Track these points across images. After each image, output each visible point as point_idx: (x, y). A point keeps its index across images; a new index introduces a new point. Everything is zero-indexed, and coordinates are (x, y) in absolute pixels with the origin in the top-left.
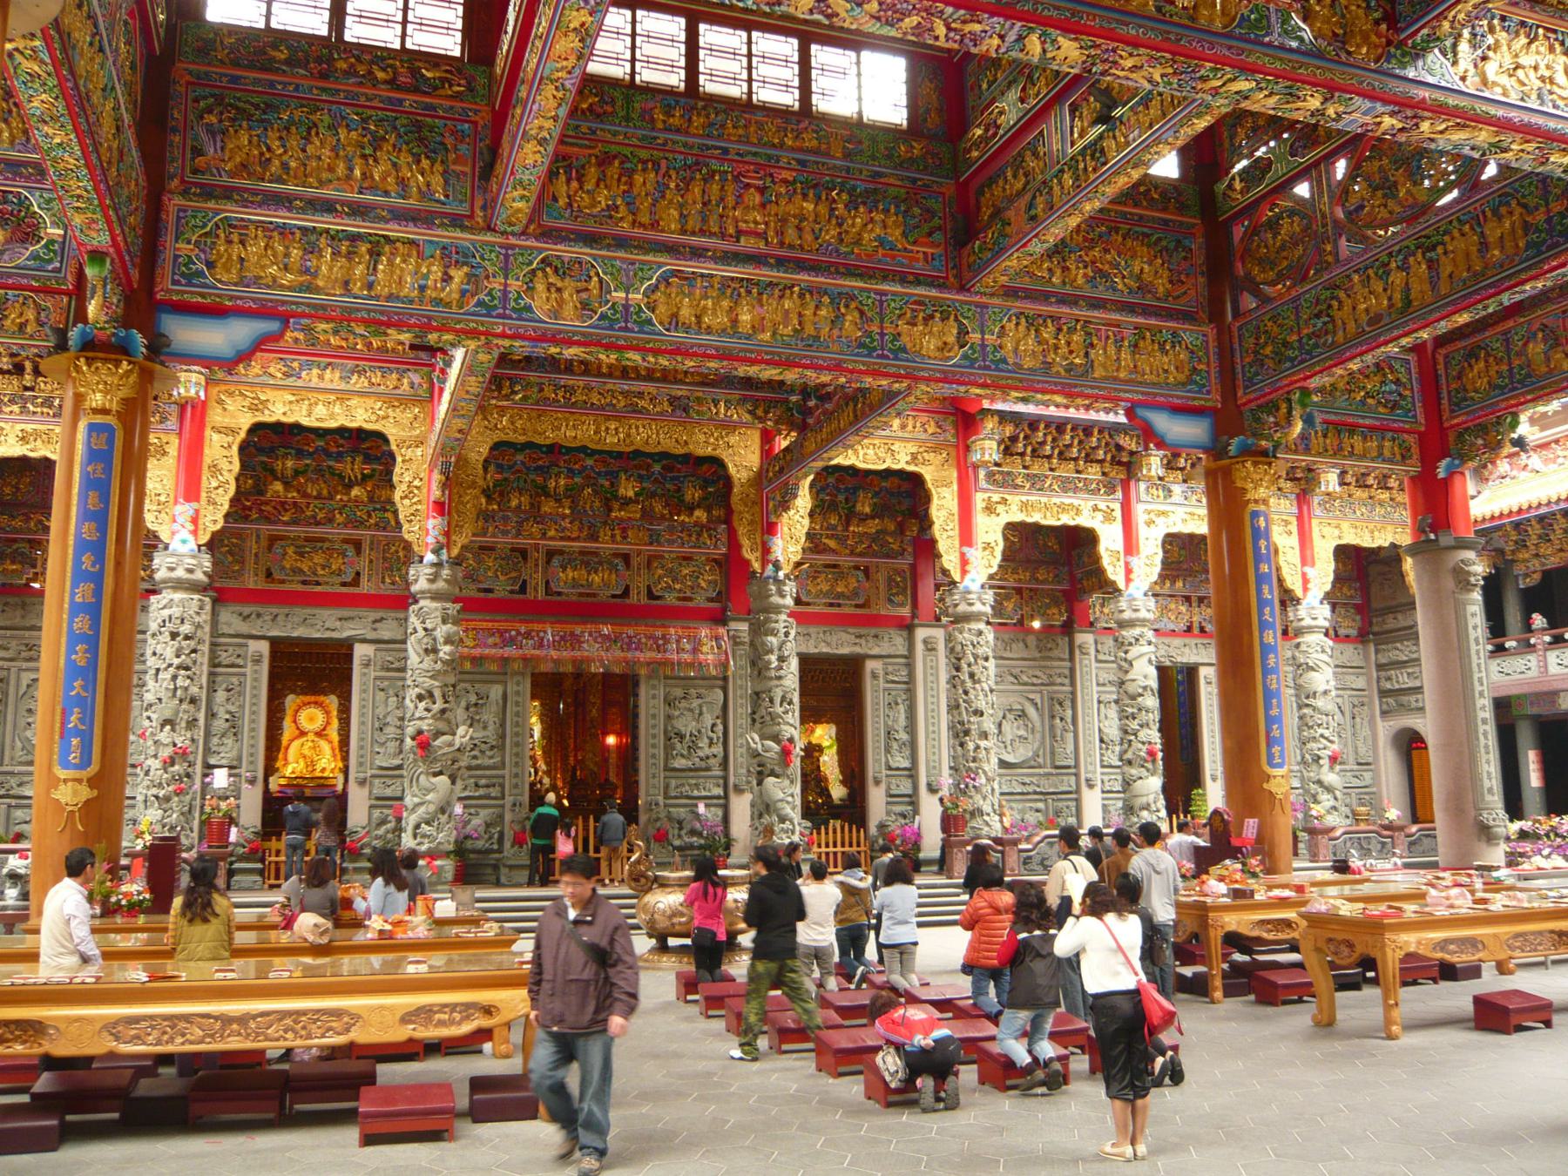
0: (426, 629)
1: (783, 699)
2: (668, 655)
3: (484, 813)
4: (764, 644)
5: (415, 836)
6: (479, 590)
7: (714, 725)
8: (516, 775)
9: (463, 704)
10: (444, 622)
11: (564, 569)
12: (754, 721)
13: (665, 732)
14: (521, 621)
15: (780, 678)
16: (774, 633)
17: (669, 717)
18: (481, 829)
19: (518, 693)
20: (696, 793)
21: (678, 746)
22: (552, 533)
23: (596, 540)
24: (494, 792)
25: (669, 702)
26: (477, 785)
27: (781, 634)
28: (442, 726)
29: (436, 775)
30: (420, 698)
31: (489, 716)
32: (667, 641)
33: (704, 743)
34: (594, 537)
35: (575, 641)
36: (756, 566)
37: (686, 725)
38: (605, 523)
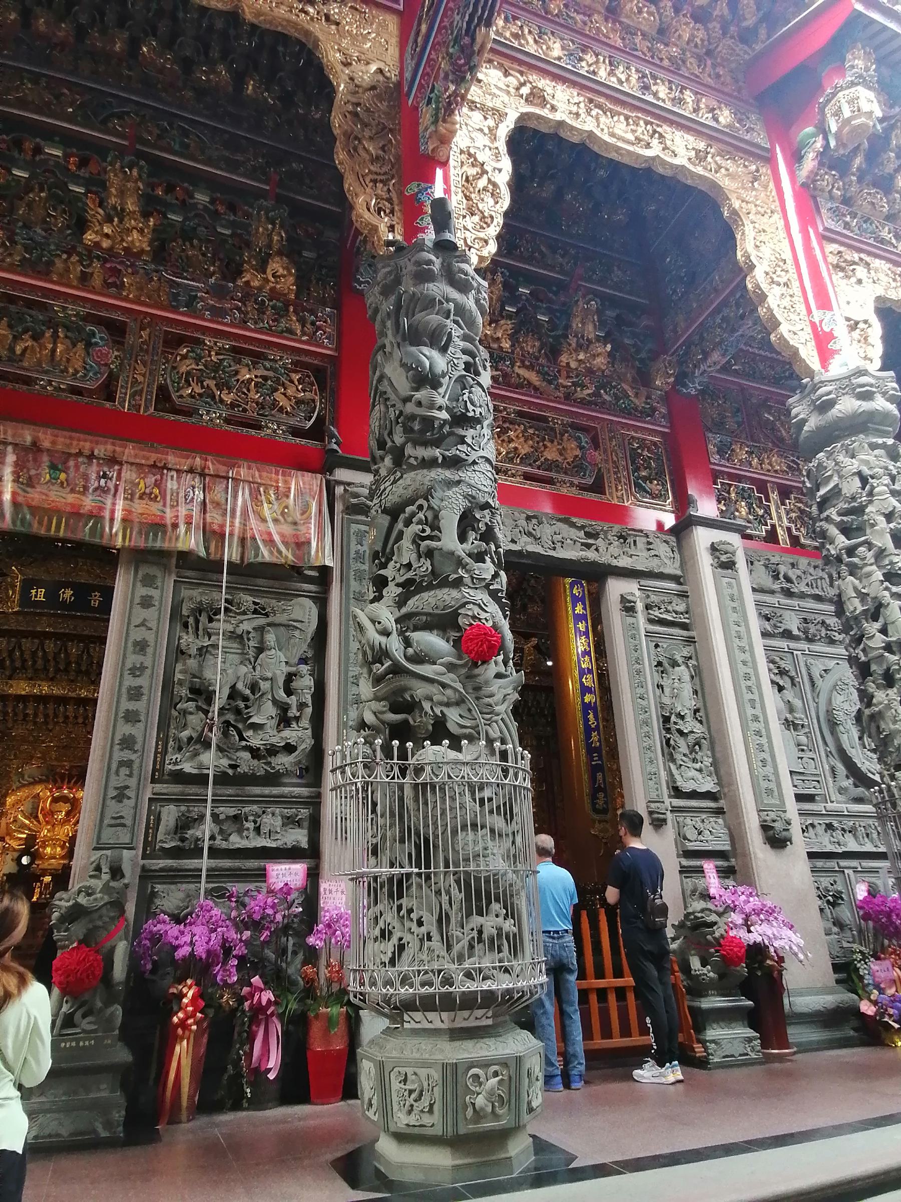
1: (466, 522)
7: (290, 678)
13: (168, 684)
23: (45, 274)
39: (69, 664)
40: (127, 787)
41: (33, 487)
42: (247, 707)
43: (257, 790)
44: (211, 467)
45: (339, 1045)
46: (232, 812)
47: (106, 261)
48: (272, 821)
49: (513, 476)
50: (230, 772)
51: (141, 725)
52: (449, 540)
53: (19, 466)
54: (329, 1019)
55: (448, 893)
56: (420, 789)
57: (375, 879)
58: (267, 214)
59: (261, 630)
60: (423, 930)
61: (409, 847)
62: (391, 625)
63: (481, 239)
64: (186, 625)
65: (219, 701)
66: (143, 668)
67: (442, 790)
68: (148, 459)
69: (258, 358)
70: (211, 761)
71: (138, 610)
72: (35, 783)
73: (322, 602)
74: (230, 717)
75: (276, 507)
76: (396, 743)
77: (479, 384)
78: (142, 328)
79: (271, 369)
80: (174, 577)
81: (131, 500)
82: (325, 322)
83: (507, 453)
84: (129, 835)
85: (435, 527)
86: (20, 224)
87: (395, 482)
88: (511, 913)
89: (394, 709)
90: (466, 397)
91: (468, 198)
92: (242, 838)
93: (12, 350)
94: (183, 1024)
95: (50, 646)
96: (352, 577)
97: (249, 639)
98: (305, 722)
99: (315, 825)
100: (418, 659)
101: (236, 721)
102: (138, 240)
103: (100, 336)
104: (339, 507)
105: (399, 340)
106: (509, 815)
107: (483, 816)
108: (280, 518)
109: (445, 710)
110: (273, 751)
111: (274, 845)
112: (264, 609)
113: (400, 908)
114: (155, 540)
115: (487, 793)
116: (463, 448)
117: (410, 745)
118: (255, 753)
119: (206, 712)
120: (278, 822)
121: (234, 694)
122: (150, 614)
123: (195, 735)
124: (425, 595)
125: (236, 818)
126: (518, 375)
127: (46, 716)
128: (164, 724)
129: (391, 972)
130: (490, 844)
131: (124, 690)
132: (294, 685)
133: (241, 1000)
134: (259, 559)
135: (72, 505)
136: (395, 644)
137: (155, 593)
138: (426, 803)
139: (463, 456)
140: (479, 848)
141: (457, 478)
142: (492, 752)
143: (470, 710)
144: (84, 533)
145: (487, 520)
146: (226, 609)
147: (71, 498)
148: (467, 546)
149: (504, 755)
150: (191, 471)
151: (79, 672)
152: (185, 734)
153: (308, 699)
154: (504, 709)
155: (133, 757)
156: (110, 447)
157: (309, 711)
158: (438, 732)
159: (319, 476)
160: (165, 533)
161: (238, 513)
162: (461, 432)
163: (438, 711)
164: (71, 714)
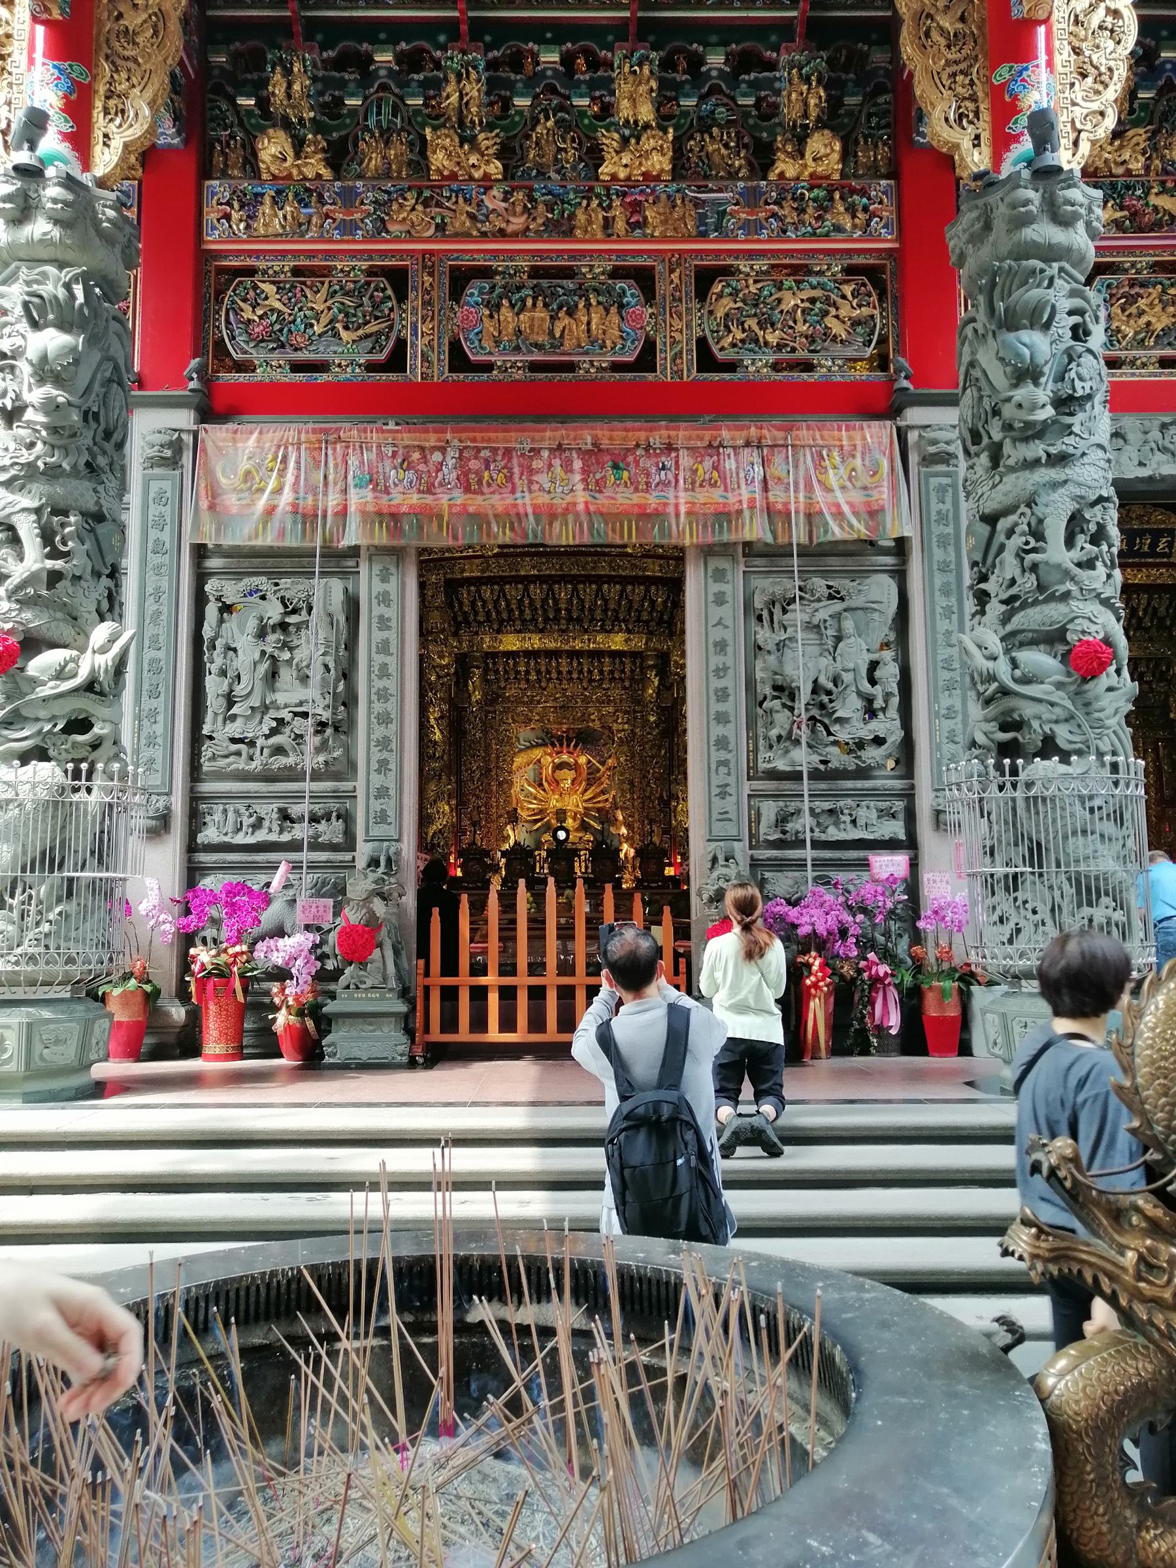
1: (1075, 524)
6: (296, 367)
7: (873, 666)
9: (252, 625)
11: (494, 308)
12: (982, 598)
13: (751, 684)
19: (384, 599)
22: (461, 222)
23: (569, 233)
24: (331, 831)
31: (313, 646)
33: (849, 707)
34: (562, 227)
36: (977, 159)
38: (588, 194)
39: (558, 611)
41: (600, 492)
42: (831, 701)
43: (849, 784)
44: (770, 435)
45: (953, 1012)
46: (827, 805)
47: (625, 194)
48: (867, 813)
49: (1144, 365)
50: (822, 767)
51: (731, 726)
52: (1056, 552)
53: (586, 471)
54: (942, 992)
55: (1060, 888)
56: (1032, 802)
57: (992, 875)
58: (800, 69)
59: (837, 617)
60: (1038, 917)
61: (1023, 849)
62: (996, 646)
63: (1095, 112)
64: (760, 618)
65: (805, 695)
67: (1053, 800)
68: (702, 439)
69: (800, 271)
70: (803, 758)
71: (713, 608)
72: (532, 747)
73: (900, 575)
74: (815, 712)
75: (842, 471)
76: (1007, 761)
77: (1089, 351)
78: (672, 271)
79: (820, 286)
80: (742, 568)
81: (693, 490)
82: (881, 203)
83: (1136, 333)
85: (1039, 536)
86: (534, 172)
87: (994, 486)
88: (1120, 905)
89: (1004, 728)
90: (1073, 374)
91: (1077, 51)
93: (551, 333)
94: (815, 985)
95: (536, 591)
96: (935, 545)
98: (893, 712)
99: (910, 817)
100: (1026, 680)
102: (660, 162)
103: (630, 291)
104: (913, 458)
105: (993, 327)
106: (1119, 818)
107: (1092, 822)
108: (848, 484)
109: (1054, 726)
110: (860, 744)
113: (1016, 899)
114: (721, 532)
115: (1097, 803)
116: (1070, 440)
117: (1020, 761)
119: (792, 709)
121: (816, 689)
122: (725, 611)
123: (784, 733)
124: (1030, 611)
125: (831, 812)
126: (1156, 208)
127: (539, 672)
128: (751, 724)
129: (1009, 949)
130: (1099, 846)
131: (712, 693)
132: (878, 674)
133: (859, 971)
134: (830, 538)
135: (639, 506)
136: (1002, 668)
137: (726, 588)
138: (1037, 813)
139: (1071, 450)
140: (1089, 851)
141: (1064, 477)
142: (1103, 765)
143: (1079, 726)
144: (655, 536)
146: (801, 598)
147: (636, 498)
148: (1075, 554)
149: (1115, 767)
150: (748, 444)
151: (570, 619)
152: (774, 733)
153: (894, 688)
154: (1115, 722)
155: (729, 756)
156: (664, 433)
157: (895, 701)
158: (1049, 748)
159: (888, 423)
160: (729, 522)
161: (802, 486)
162: (1068, 420)
163: (1047, 729)
164: (564, 669)
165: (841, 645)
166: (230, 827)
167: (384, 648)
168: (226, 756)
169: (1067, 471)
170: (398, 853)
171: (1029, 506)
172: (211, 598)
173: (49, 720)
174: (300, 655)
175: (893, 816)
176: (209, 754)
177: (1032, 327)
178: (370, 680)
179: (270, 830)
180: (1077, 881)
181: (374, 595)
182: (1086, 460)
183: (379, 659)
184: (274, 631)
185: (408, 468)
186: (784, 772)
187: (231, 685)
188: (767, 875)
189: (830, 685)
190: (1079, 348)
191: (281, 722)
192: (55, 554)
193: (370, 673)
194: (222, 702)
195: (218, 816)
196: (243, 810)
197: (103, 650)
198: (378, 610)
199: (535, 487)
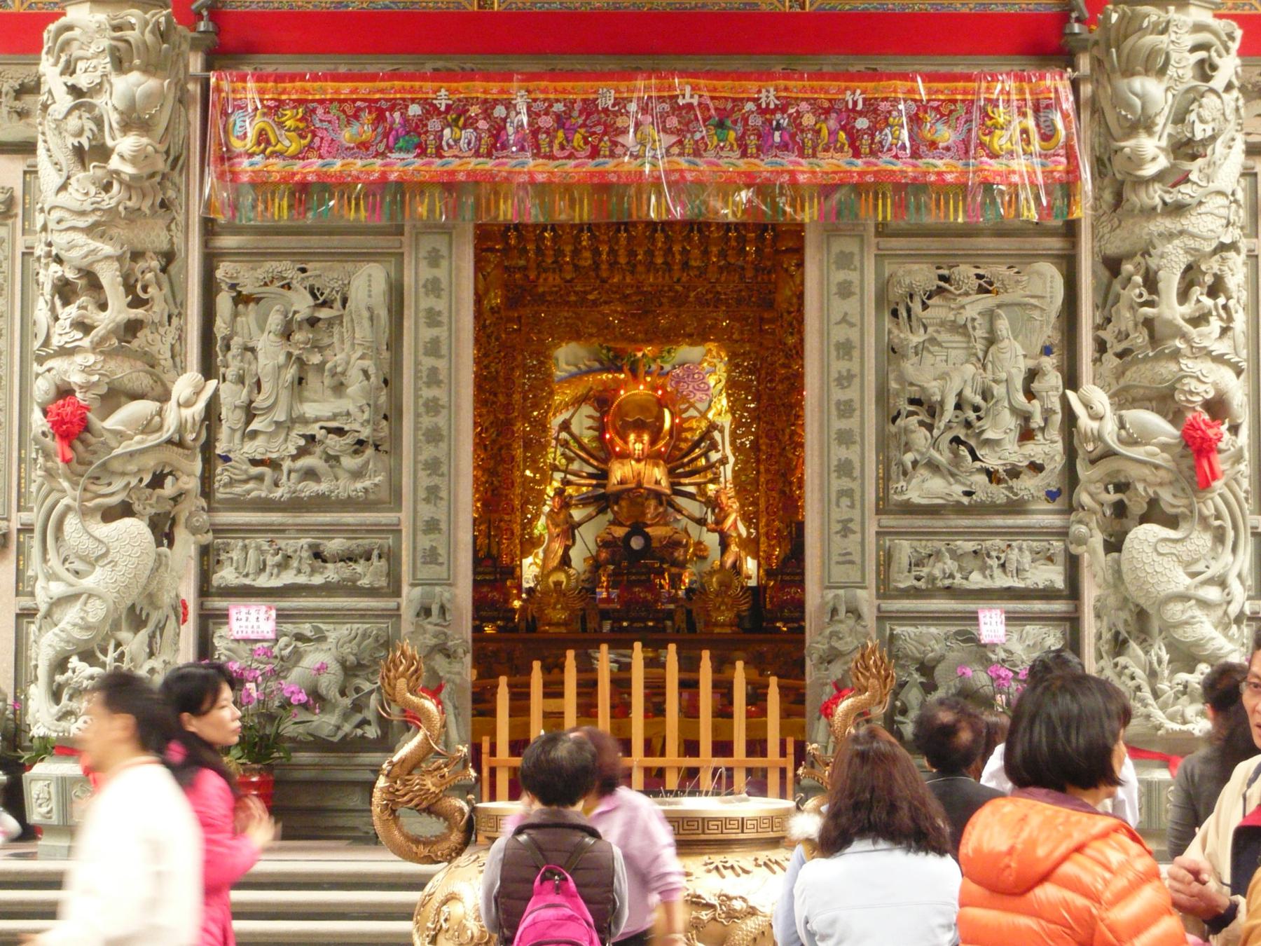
0: (74, 90)
1: (1190, 276)
2: (884, 162)
3: (337, 633)
4: (1119, 101)
5: (56, 696)
8: (432, 526)
9: (275, 320)
10: (120, 63)
13: (883, 395)
14: (437, 75)
15: (1179, 209)
16: (1157, 65)
17: (893, 352)
18: (329, 684)
19: (434, 287)
20: (977, 580)
21: (921, 437)
24: (367, 573)
25: (894, 307)
26: (317, 555)
27: (1184, 64)
28: (125, 371)
29: (109, 515)
30: (65, 291)
31: (351, 353)
32: (880, 120)
33: (1001, 427)
35: (601, 128)
37: (946, 373)
40: (851, 520)
41: (700, 156)
42: (979, 418)
43: (998, 521)
46: (970, 546)
48: (1020, 554)
50: (965, 500)
64: (895, 313)
66: (850, 376)
77: (1212, 90)
84: (859, 573)
92: (985, 577)
97: (974, 328)
98: (1055, 433)
100: (1133, 442)
101: (967, 435)
110: (1014, 473)
111: (1022, 585)
112: (991, 284)
116: (1185, 188)
118: (991, 475)
119: (930, 428)
120: (1027, 558)
128: (883, 443)
132: (1035, 386)
137: (853, 276)
139: (1188, 200)
141: (1179, 227)
145: (1216, 269)
148: (1188, 309)
152: (909, 458)
162: (1187, 165)
163: (1151, 492)
165: (993, 349)
166: (251, 567)
167: (433, 349)
168: (246, 481)
169: (1184, 221)
170: (453, 599)
171: (1143, 255)
172: (224, 286)
173: (135, 474)
174: (337, 359)
175: (1050, 559)
176: (225, 479)
177: (1147, 72)
178: (417, 389)
179: (299, 571)
180: (1172, 646)
181: (421, 283)
182: (1203, 209)
183: (428, 362)
184: (300, 328)
185: (465, 127)
186: (920, 505)
187: (250, 392)
188: (898, 630)
189: (978, 400)
190: (1203, 87)
191: (311, 439)
192: (137, 303)
193: (417, 378)
194: (240, 415)
195: (236, 555)
196: (265, 547)
197: (188, 404)
198: (426, 303)
199: (619, 150)
